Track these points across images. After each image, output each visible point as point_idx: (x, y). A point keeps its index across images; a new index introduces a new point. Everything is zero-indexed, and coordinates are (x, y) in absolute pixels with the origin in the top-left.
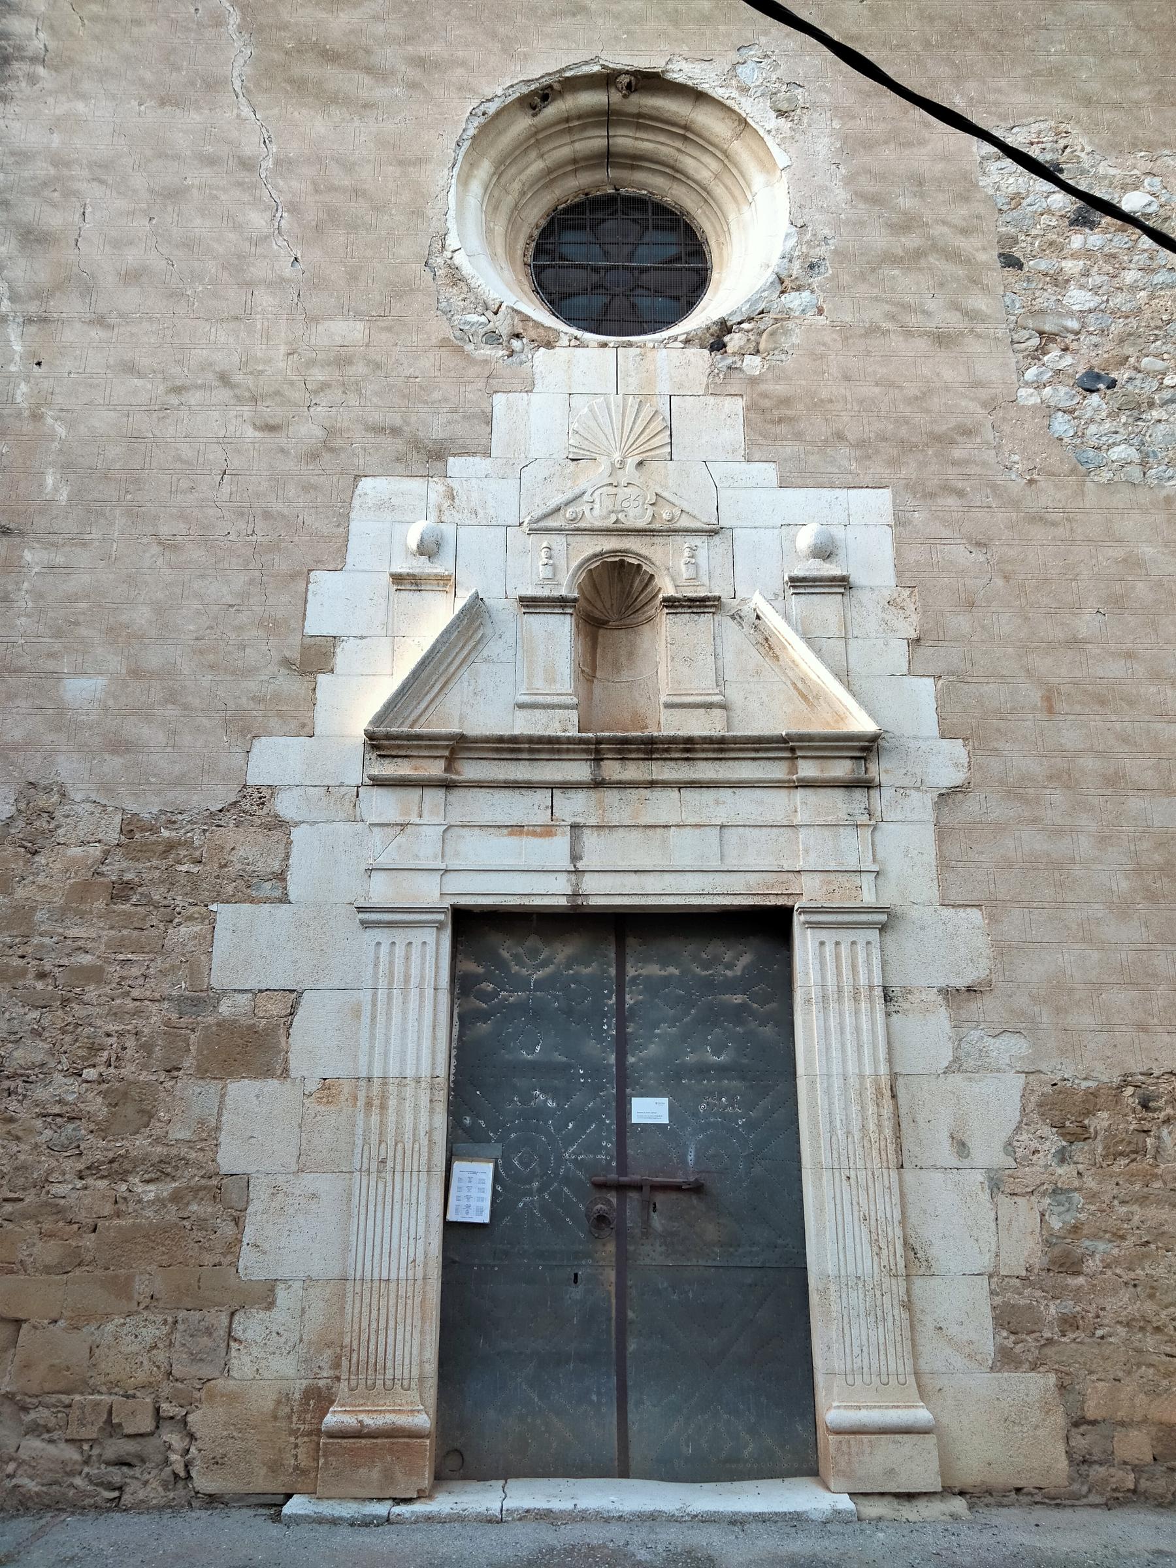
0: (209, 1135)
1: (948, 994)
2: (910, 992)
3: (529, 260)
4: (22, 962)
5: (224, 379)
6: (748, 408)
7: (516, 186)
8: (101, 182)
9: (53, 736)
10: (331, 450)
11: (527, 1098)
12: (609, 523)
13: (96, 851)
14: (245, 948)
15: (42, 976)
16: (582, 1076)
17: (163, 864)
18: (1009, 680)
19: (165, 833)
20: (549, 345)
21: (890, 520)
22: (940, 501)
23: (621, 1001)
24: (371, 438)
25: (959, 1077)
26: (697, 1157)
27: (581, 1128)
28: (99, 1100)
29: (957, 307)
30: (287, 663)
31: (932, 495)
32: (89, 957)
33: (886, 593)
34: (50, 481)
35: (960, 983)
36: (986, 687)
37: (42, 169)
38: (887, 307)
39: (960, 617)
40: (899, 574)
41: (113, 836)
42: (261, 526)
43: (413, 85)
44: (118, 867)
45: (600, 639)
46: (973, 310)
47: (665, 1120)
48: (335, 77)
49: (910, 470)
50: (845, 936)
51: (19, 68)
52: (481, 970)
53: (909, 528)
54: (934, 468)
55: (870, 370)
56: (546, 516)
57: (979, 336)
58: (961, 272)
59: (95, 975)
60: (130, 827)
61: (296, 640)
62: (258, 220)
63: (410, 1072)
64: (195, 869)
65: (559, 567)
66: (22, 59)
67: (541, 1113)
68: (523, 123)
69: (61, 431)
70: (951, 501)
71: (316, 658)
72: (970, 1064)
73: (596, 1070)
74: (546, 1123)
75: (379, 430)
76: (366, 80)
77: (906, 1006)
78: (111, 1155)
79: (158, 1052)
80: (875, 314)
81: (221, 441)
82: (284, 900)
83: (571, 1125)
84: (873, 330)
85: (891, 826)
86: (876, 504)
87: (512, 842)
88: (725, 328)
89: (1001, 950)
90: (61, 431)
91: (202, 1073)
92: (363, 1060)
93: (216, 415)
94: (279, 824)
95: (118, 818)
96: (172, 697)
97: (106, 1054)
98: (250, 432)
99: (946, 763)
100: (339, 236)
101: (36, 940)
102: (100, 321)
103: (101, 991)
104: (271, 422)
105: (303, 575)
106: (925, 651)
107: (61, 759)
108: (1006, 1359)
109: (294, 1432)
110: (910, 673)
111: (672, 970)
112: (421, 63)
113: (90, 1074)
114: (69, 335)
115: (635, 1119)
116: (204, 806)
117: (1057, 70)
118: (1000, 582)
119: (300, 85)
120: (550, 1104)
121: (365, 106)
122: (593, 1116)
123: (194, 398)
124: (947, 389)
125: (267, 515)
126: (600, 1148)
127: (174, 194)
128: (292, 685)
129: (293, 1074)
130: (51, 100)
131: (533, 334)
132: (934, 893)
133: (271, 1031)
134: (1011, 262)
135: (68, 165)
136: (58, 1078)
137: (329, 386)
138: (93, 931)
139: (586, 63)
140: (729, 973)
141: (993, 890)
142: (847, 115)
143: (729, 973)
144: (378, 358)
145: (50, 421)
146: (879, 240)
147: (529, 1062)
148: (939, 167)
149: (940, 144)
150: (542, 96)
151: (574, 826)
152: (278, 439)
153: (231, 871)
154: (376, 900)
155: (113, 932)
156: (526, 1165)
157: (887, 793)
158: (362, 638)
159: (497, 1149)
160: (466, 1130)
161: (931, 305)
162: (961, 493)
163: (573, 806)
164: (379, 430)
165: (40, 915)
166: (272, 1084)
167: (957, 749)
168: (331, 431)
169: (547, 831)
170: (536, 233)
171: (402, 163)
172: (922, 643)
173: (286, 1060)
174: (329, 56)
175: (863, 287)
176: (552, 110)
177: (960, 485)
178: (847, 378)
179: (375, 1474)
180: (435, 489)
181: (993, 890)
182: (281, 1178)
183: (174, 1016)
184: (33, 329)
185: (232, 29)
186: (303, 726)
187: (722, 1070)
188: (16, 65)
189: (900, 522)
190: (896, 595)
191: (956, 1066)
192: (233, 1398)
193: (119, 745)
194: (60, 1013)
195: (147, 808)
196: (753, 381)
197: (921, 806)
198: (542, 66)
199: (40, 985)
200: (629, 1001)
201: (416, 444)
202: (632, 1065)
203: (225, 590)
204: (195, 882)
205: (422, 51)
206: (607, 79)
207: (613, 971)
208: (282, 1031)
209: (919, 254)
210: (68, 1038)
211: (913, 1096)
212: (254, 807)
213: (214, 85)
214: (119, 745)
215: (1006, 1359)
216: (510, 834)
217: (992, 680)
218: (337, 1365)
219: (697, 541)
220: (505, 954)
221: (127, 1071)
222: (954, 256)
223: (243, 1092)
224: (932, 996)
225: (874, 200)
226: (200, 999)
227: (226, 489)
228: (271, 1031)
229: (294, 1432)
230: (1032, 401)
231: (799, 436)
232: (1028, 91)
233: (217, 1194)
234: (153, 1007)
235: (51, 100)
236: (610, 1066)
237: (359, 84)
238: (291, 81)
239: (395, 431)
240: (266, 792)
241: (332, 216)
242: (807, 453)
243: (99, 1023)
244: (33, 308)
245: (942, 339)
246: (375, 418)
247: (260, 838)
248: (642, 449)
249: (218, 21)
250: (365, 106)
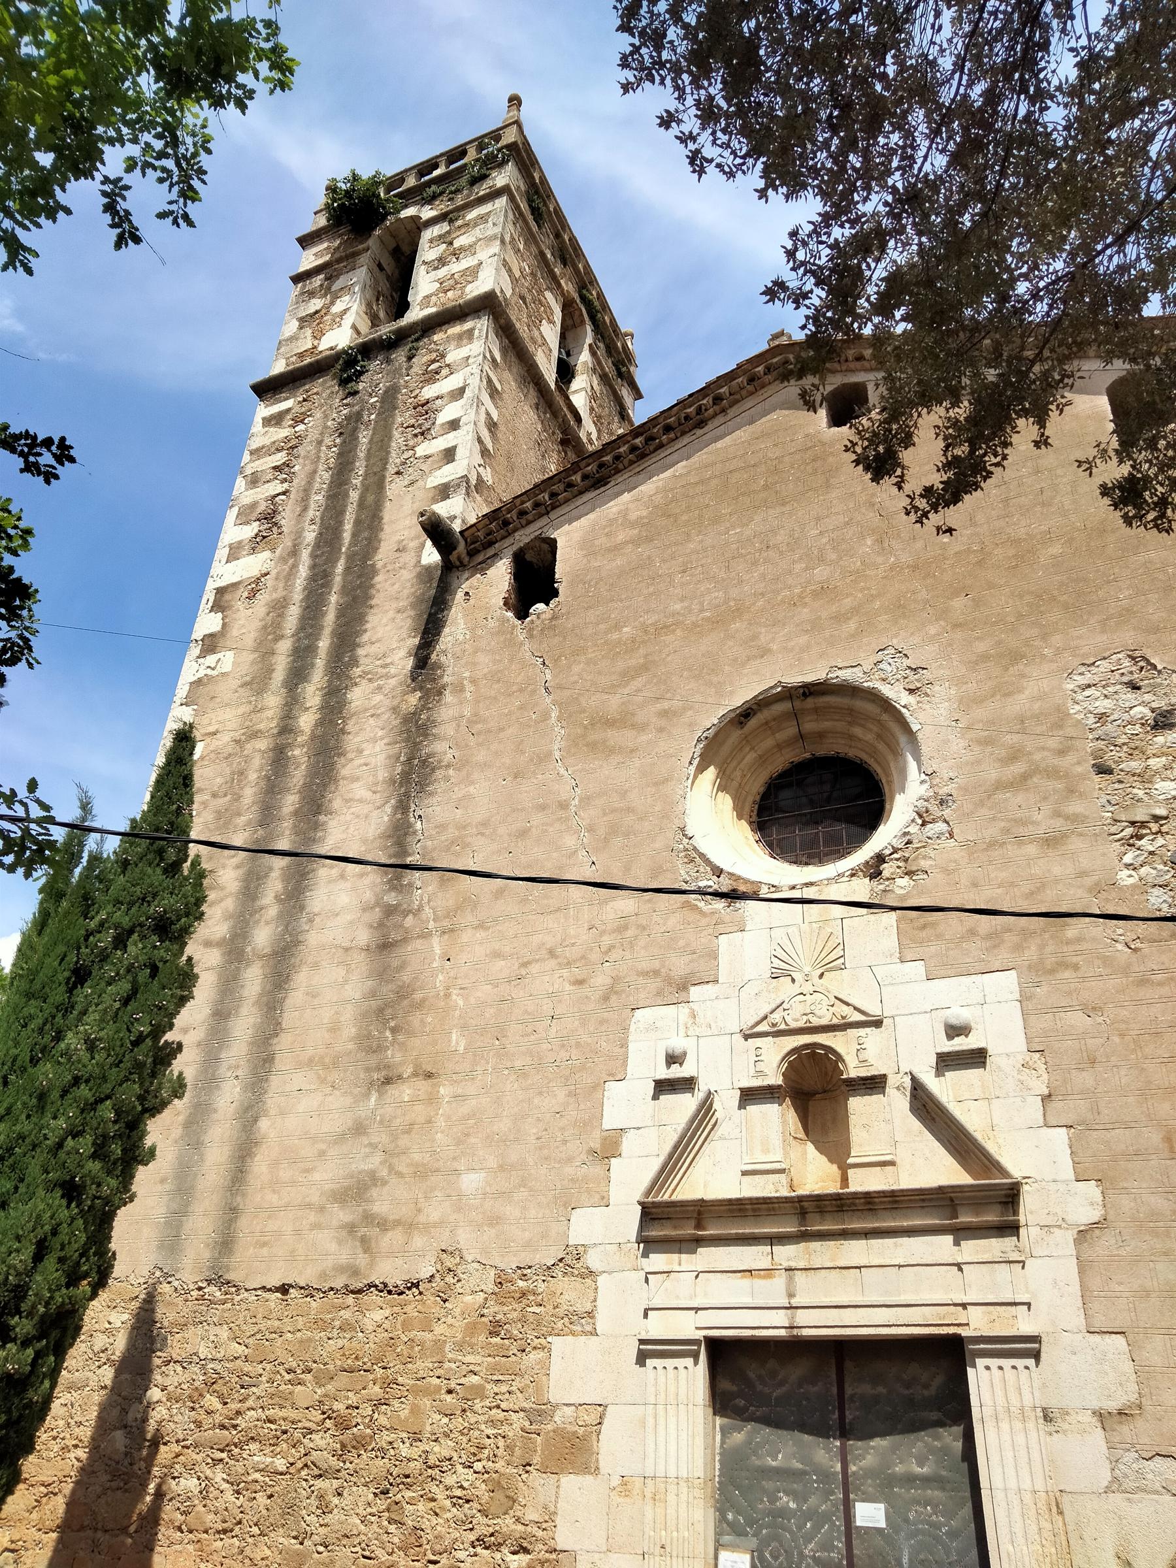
0: (549, 1519)
1: (1101, 1416)
2: (1068, 1414)
3: (755, 818)
4: (438, 1381)
5: (552, 953)
7: (738, 773)
8: (483, 834)
9: (455, 1216)
10: (616, 993)
11: (773, 1499)
12: (801, 1024)
16: (815, 1481)
18: (1133, 1125)
19: (521, 1284)
21: (1017, 996)
22: (1060, 975)
23: (842, 1417)
24: (641, 980)
25: (1119, 1497)
26: (910, 1559)
27: (817, 1528)
28: (483, 1486)
29: (1057, 814)
31: (1052, 971)
32: (477, 1378)
33: (1020, 1059)
35: (1113, 1405)
36: (1113, 1133)
37: (452, 832)
38: (1003, 824)
39: (1084, 1074)
40: (1029, 1040)
41: (490, 1287)
42: (575, 1054)
43: (661, 730)
45: (810, 1108)
46: (1074, 814)
47: (882, 1524)
48: (614, 736)
49: (1031, 952)
50: (1007, 1363)
51: (439, 774)
52: (734, 1388)
53: (1035, 1001)
54: (1050, 949)
55: (992, 875)
56: (758, 1023)
57: (1081, 835)
58: (1059, 786)
59: (479, 1392)
61: (597, 1134)
62: (570, 841)
63: (672, 1473)
64: (537, 1310)
65: (769, 1063)
66: (440, 768)
67: (783, 1513)
68: (736, 735)
69: (461, 1003)
70: (1067, 974)
71: (609, 1149)
72: (1129, 1484)
73: (825, 1476)
74: (789, 1521)
75: (645, 974)
77: (1065, 1426)
78: (491, 1530)
79: (518, 1452)
80: (992, 832)
81: (551, 995)
83: (809, 1525)
84: (992, 844)
85: (1039, 1261)
86: (1006, 984)
87: (745, 1282)
88: (880, 859)
89: (1143, 1373)
90: (461, 1003)
92: (650, 1461)
93: (547, 978)
95: (493, 1272)
96: (523, 1183)
97: (486, 1451)
98: (568, 987)
99: (1085, 1204)
100: (618, 841)
101: (447, 1365)
103: (483, 1404)
104: (579, 978)
105: (598, 1087)
106: (1056, 1105)
107: (460, 1231)
110: (1046, 1125)
111: (881, 1390)
113: (478, 1466)
114: (466, 936)
115: (859, 1522)
116: (543, 1262)
117: (1128, 610)
118: (1117, 1039)
119: (593, 746)
120: (792, 1505)
121: (632, 751)
122: (826, 1517)
123: (534, 968)
124: (1057, 881)
125: (578, 1045)
126: (833, 1548)
128: (597, 1170)
129: (602, 1471)
130: (456, 789)
132: (1079, 1321)
133: (584, 1439)
134: (1103, 770)
135: (464, 827)
136: (459, 1468)
137: (614, 947)
139: (771, 688)
140: (926, 1393)
141: (1134, 1318)
142: (960, 681)
143: (926, 1393)
144: (644, 923)
145: (454, 997)
146: (992, 773)
147: (774, 1468)
148: (1036, 706)
149: (1036, 688)
150: (745, 714)
152: (585, 990)
153: (560, 1312)
154: (654, 1334)
155: (489, 1359)
156: (776, 1558)
157: (1034, 1231)
158: (639, 1128)
159: (753, 1542)
160: (728, 1523)
161: (1037, 817)
162: (1076, 967)
163: (787, 1254)
164: (645, 974)
166: (589, 1478)
167: (1092, 1190)
168: (616, 979)
169: (768, 1272)
170: (758, 798)
171: (656, 784)
172: (1053, 1098)
173: (597, 1460)
174: (610, 723)
175: (984, 811)
176: (753, 722)
177: (1075, 959)
178: (975, 885)
180: (684, 1010)
181: (1134, 1318)
182: (597, 1556)
183: (527, 1424)
184: (446, 937)
185: (553, 720)
186: (603, 1198)
187: (926, 1480)
188: (438, 772)
189: (1024, 999)
190: (1028, 1059)
191: (1115, 1485)
193: (495, 1220)
194: (460, 1419)
195: (509, 1263)
197: (1065, 1240)
199: (449, 1398)
200: (849, 1416)
201: (668, 980)
202: (854, 1473)
203: (554, 1101)
205: (666, 705)
207: (835, 1390)
208: (594, 1437)
209: (1025, 777)
210: (465, 1439)
211: (1078, 1514)
212: (571, 1262)
213: (543, 758)
214: (495, 1220)
216: (742, 1277)
217: (1117, 1125)
220: (752, 1375)
221: (500, 1465)
222: (1053, 773)
223: (570, 1482)
224: (1088, 1418)
225: (986, 742)
226: (540, 1412)
227: (553, 1030)
228: (584, 1439)
230: (1131, 881)
231: (939, 937)
232: (1103, 631)
234: (514, 1416)
235: (456, 789)
236: (837, 1473)
238: (587, 745)
239: (656, 973)
240: (581, 1249)
241: (613, 830)
242: (948, 949)
243: (483, 1427)
244: (446, 923)
245: (1051, 842)
246: (645, 965)
247: (578, 1285)
248: (823, 963)
250: (632, 751)
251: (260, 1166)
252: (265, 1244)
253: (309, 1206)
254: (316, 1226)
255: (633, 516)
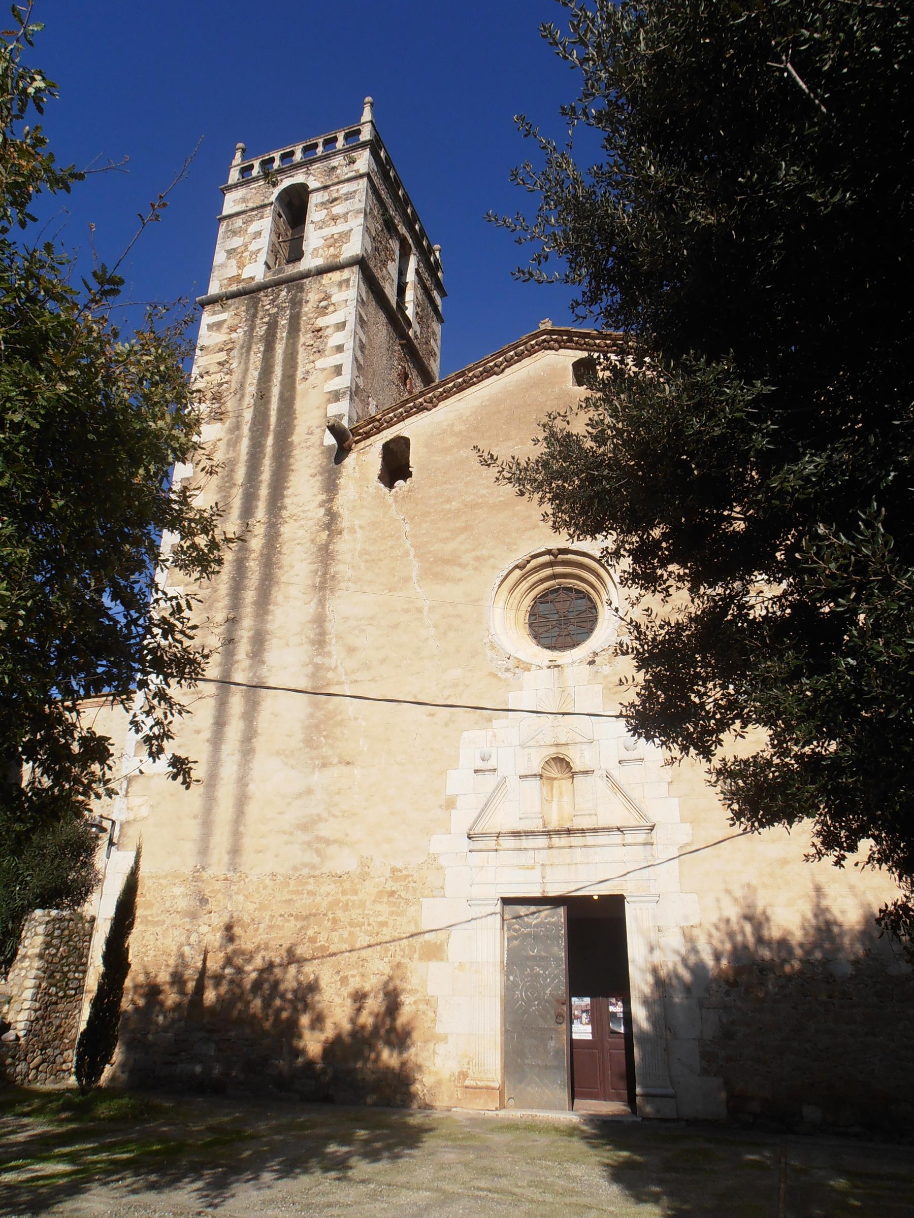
3: (527, 621)
6: (603, 689)
13: (383, 880)
14: (432, 913)
15: (369, 925)
17: (404, 884)
20: (529, 670)
30: (440, 806)
34: (361, 743)
44: (390, 886)
47: (589, 1037)
60: (394, 870)
68: (518, 573)
71: (450, 804)
76: (457, 569)
82: (444, 896)
91: (421, 959)
94: (441, 868)
102: (373, 680)
108: (705, 1072)
109: (456, 1086)
112: (477, 559)
127: (395, 626)
131: (522, 666)
133: (441, 944)
138: (384, 908)
151: (543, 865)
163: (542, 856)
165: (368, 903)
167: (687, 827)
179: (482, 1101)
185: (411, 557)
192: (436, 1073)
196: (606, 677)
198: (520, 556)
204: (415, 890)
205: (478, 553)
206: (549, 552)
213: (407, 580)
215: (705, 1072)
218: (468, 1064)
219: (584, 747)
223: (433, 966)
228: (441, 944)
229: (456, 1086)
233: (427, 1003)
237: (454, 571)
249: (407, 554)
251: (252, 810)
252: (260, 851)
253: (284, 832)
254: (287, 843)
255: (457, 429)
